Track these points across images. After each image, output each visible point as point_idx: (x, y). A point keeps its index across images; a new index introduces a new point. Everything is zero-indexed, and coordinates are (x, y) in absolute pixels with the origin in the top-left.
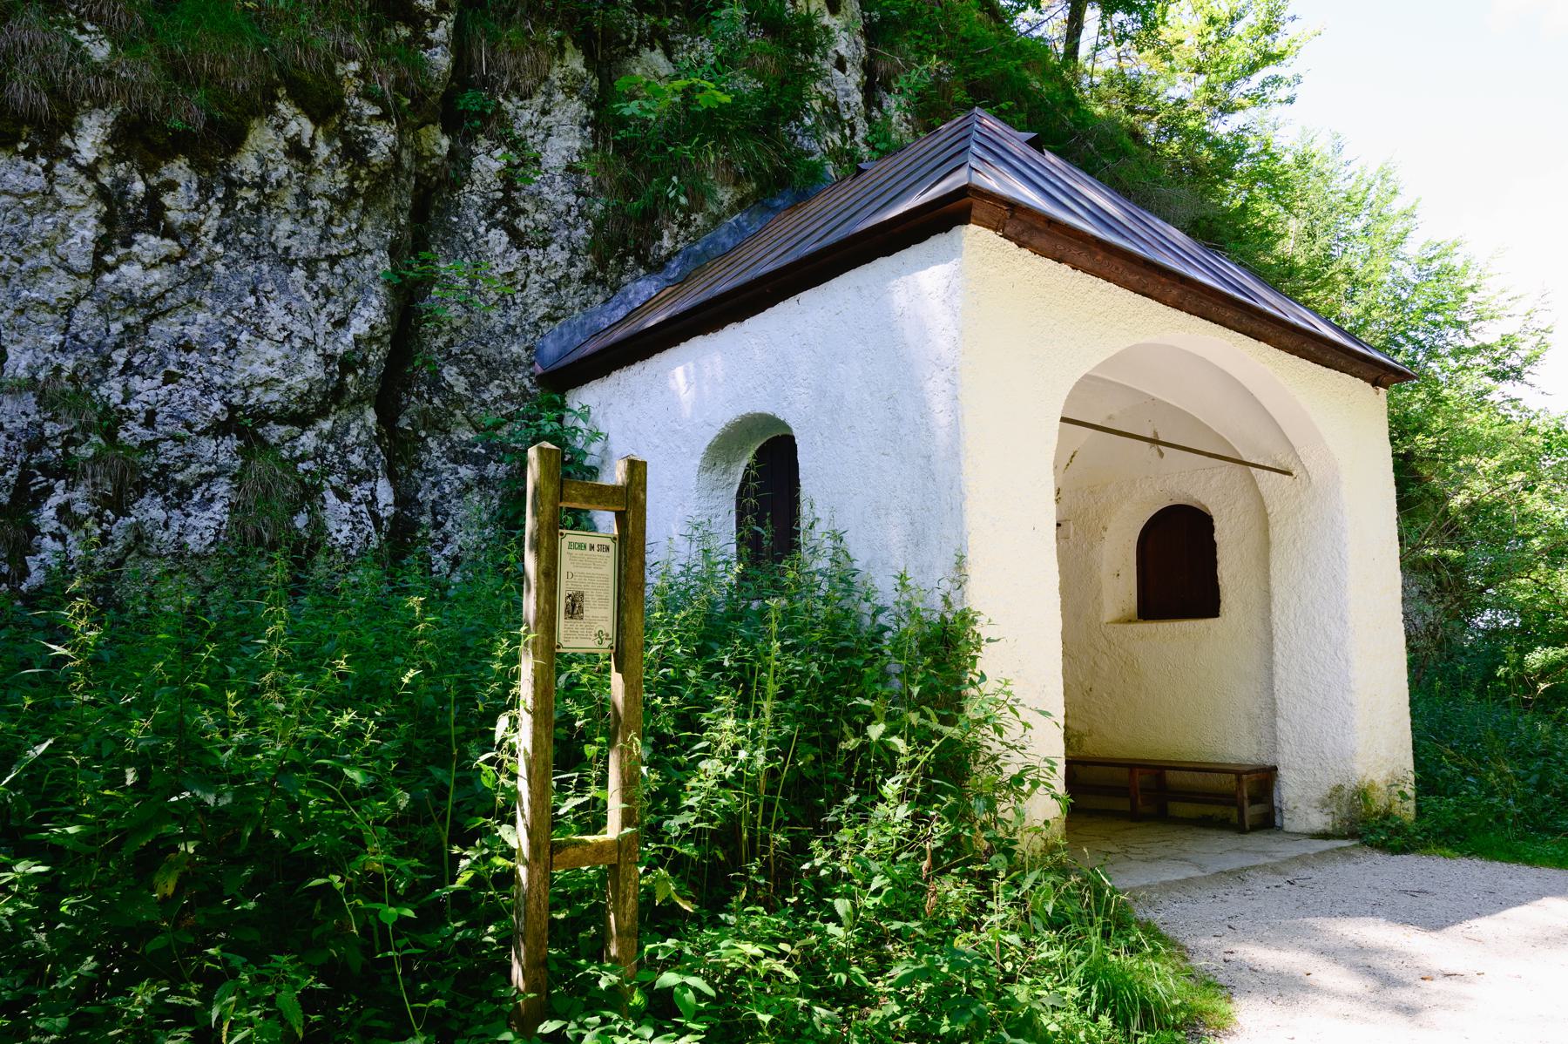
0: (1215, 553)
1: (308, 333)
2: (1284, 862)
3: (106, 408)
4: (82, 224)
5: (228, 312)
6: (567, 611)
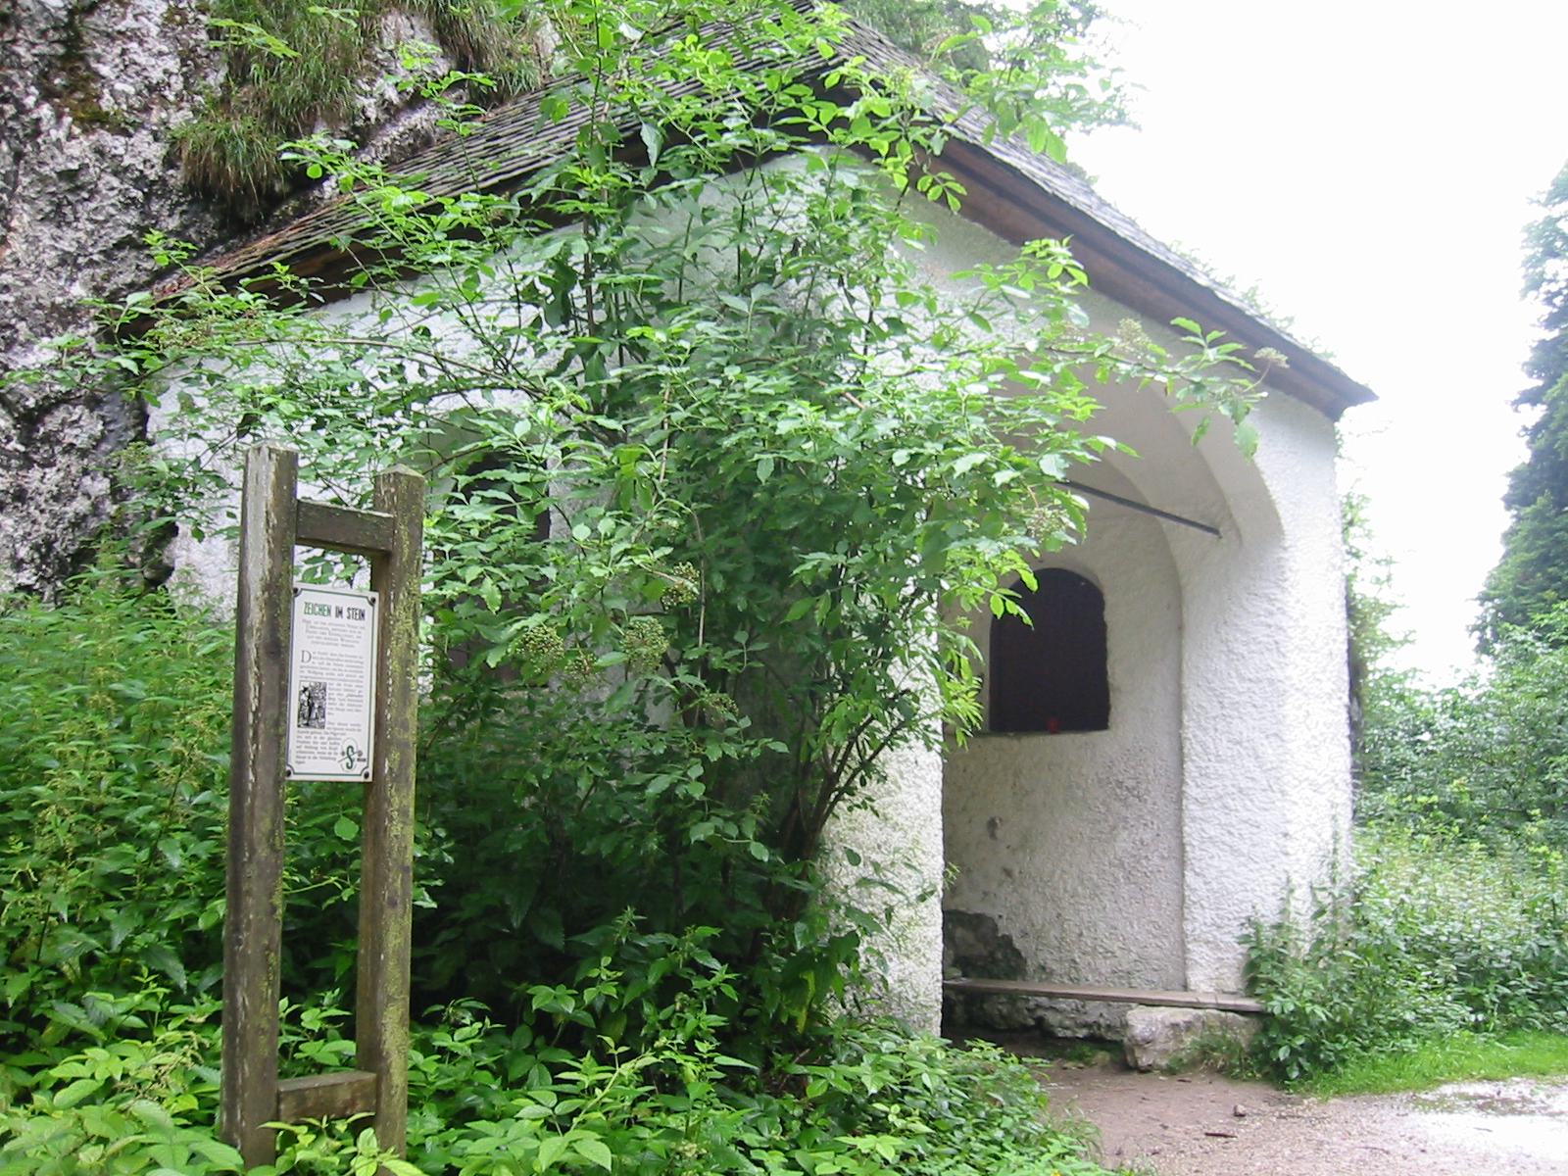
0: (1104, 639)
6: (301, 715)
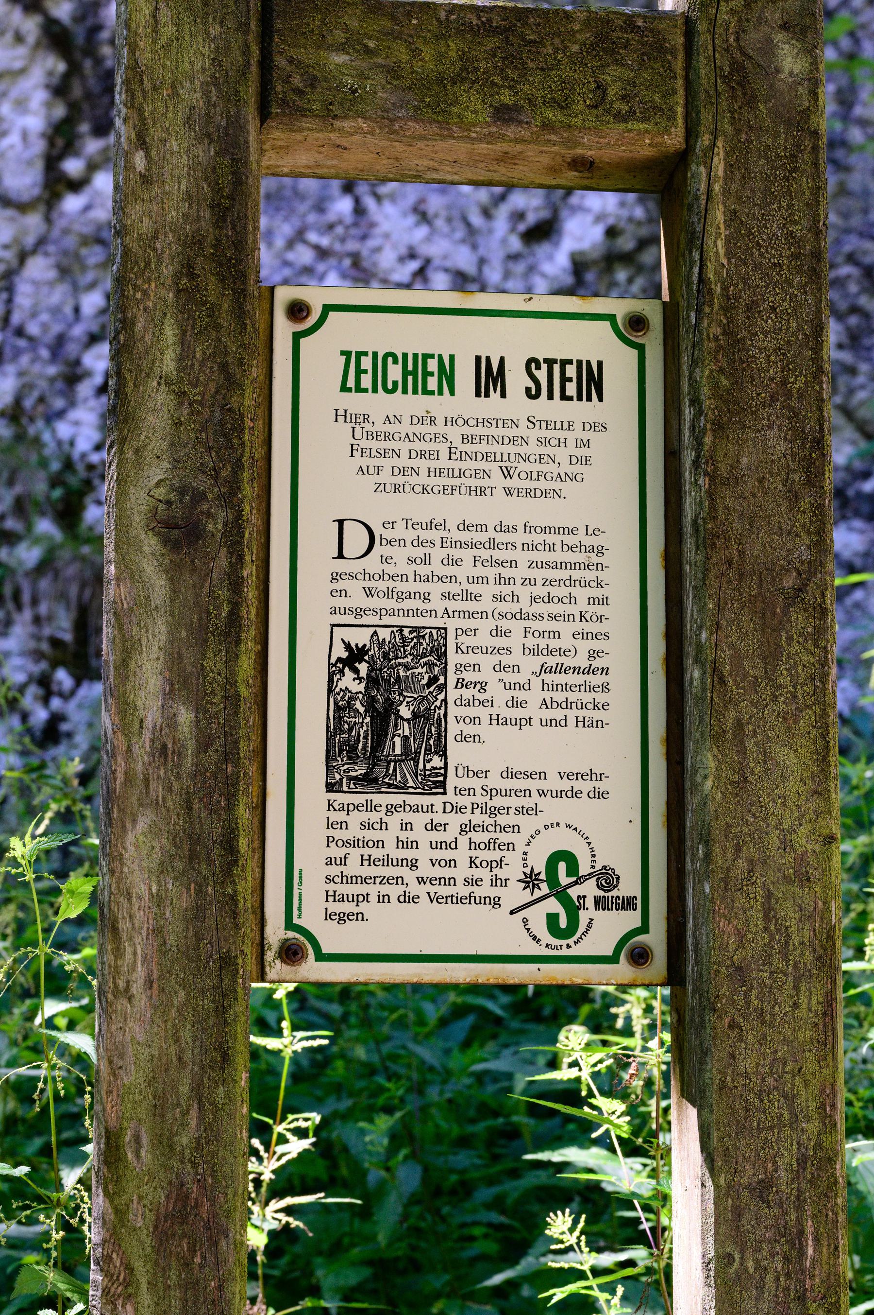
1: (464, 260)
2: (155, 31)
3: (68, 465)
4: (21, 105)
5: (299, 237)
